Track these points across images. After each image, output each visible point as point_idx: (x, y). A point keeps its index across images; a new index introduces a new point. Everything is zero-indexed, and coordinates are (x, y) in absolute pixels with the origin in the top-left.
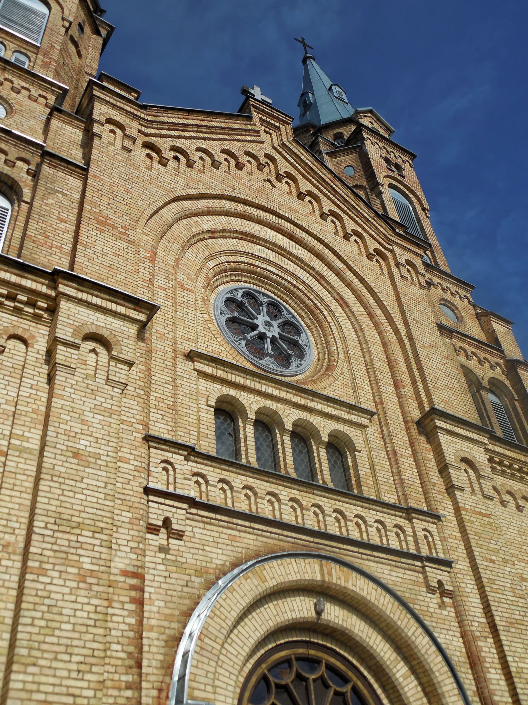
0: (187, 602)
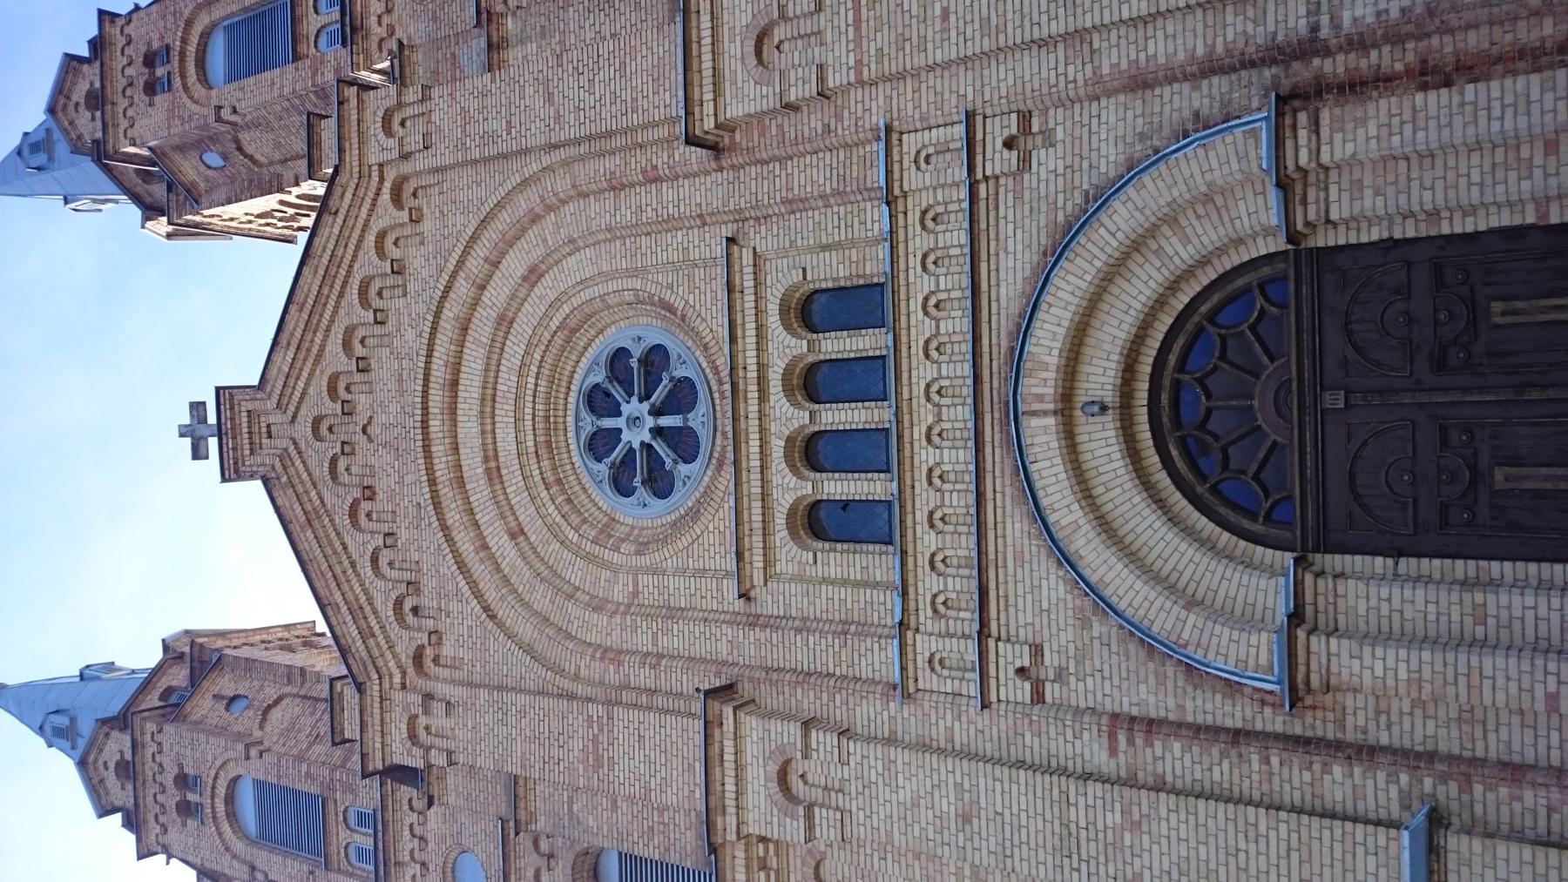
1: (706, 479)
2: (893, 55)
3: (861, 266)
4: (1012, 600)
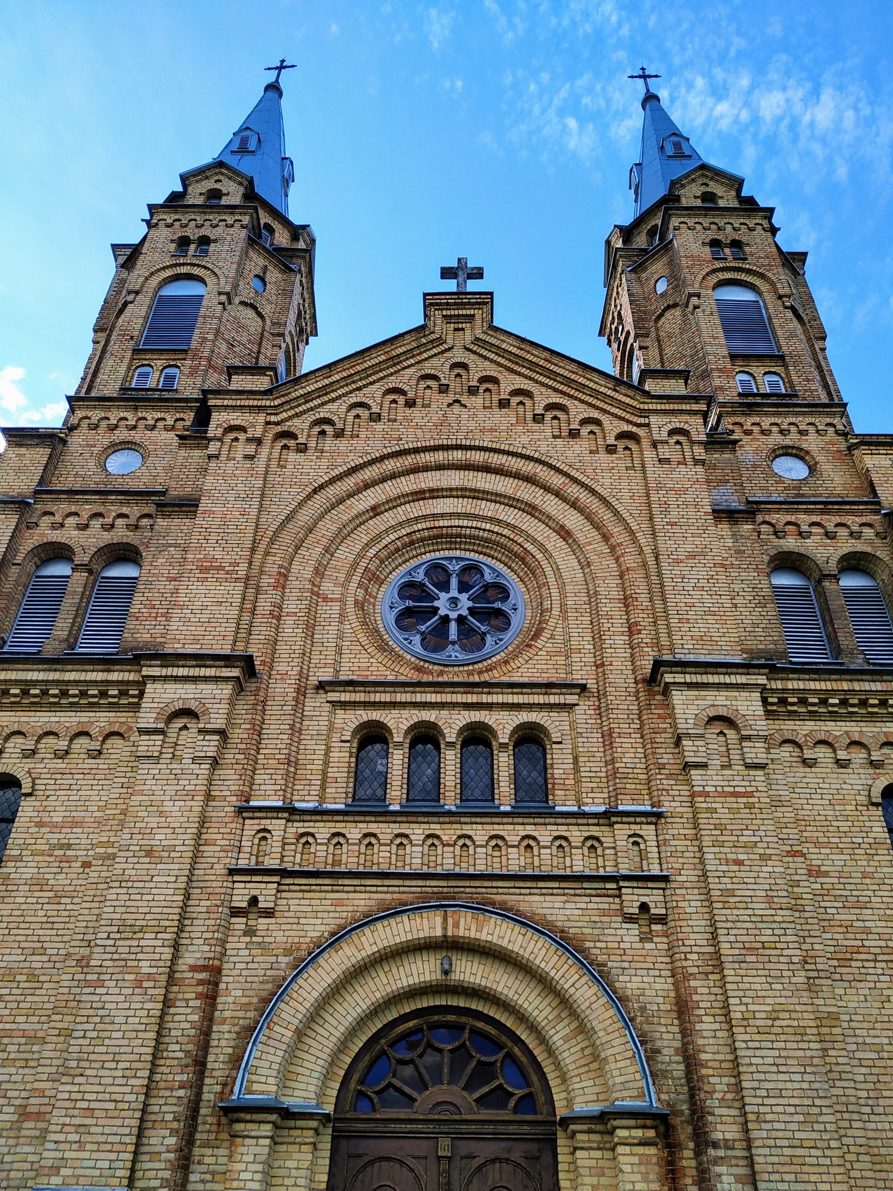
0: (270, 986)
1: (409, 657)
2: (711, 821)
3: (562, 787)
4: (307, 895)
